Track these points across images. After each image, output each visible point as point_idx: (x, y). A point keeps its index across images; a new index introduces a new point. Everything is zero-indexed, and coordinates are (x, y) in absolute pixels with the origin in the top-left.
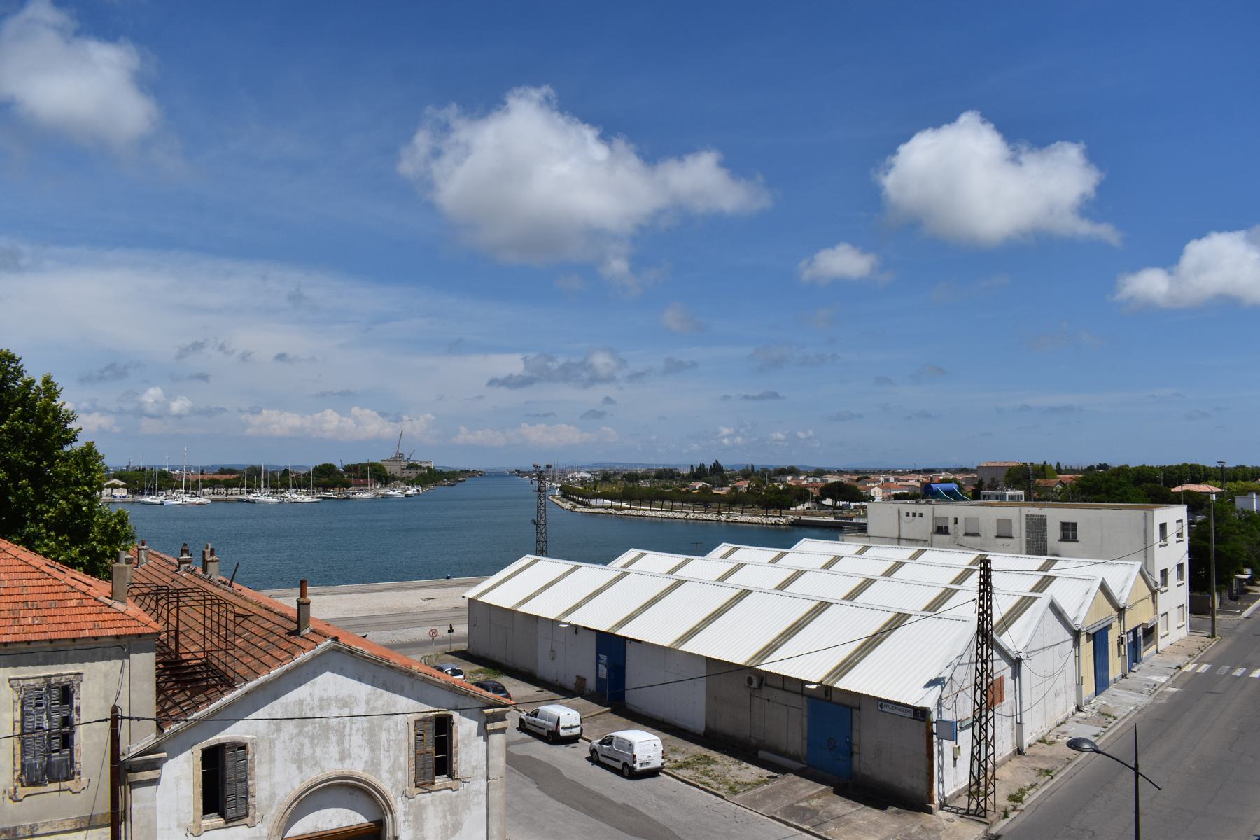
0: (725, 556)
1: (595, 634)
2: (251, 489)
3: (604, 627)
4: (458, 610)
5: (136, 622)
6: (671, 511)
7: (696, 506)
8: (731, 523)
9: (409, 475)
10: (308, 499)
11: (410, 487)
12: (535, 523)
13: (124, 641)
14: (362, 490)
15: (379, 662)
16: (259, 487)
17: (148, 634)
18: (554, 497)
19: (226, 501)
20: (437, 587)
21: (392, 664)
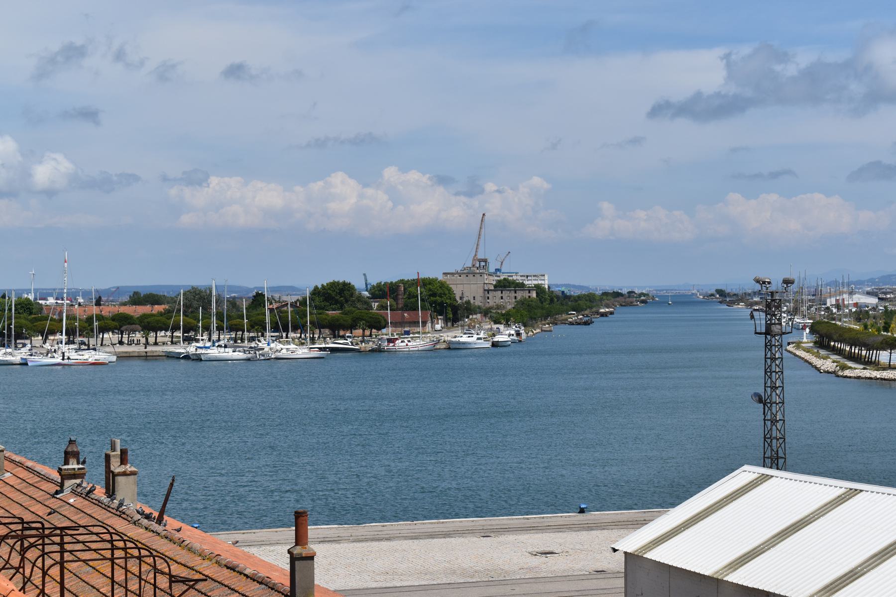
2: (192, 334)
9: (499, 302)
10: (302, 352)
11: (501, 327)
12: (760, 400)
14: (407, 333)
16: (207, 328)
19: (146, 357)
20: (560, 528)
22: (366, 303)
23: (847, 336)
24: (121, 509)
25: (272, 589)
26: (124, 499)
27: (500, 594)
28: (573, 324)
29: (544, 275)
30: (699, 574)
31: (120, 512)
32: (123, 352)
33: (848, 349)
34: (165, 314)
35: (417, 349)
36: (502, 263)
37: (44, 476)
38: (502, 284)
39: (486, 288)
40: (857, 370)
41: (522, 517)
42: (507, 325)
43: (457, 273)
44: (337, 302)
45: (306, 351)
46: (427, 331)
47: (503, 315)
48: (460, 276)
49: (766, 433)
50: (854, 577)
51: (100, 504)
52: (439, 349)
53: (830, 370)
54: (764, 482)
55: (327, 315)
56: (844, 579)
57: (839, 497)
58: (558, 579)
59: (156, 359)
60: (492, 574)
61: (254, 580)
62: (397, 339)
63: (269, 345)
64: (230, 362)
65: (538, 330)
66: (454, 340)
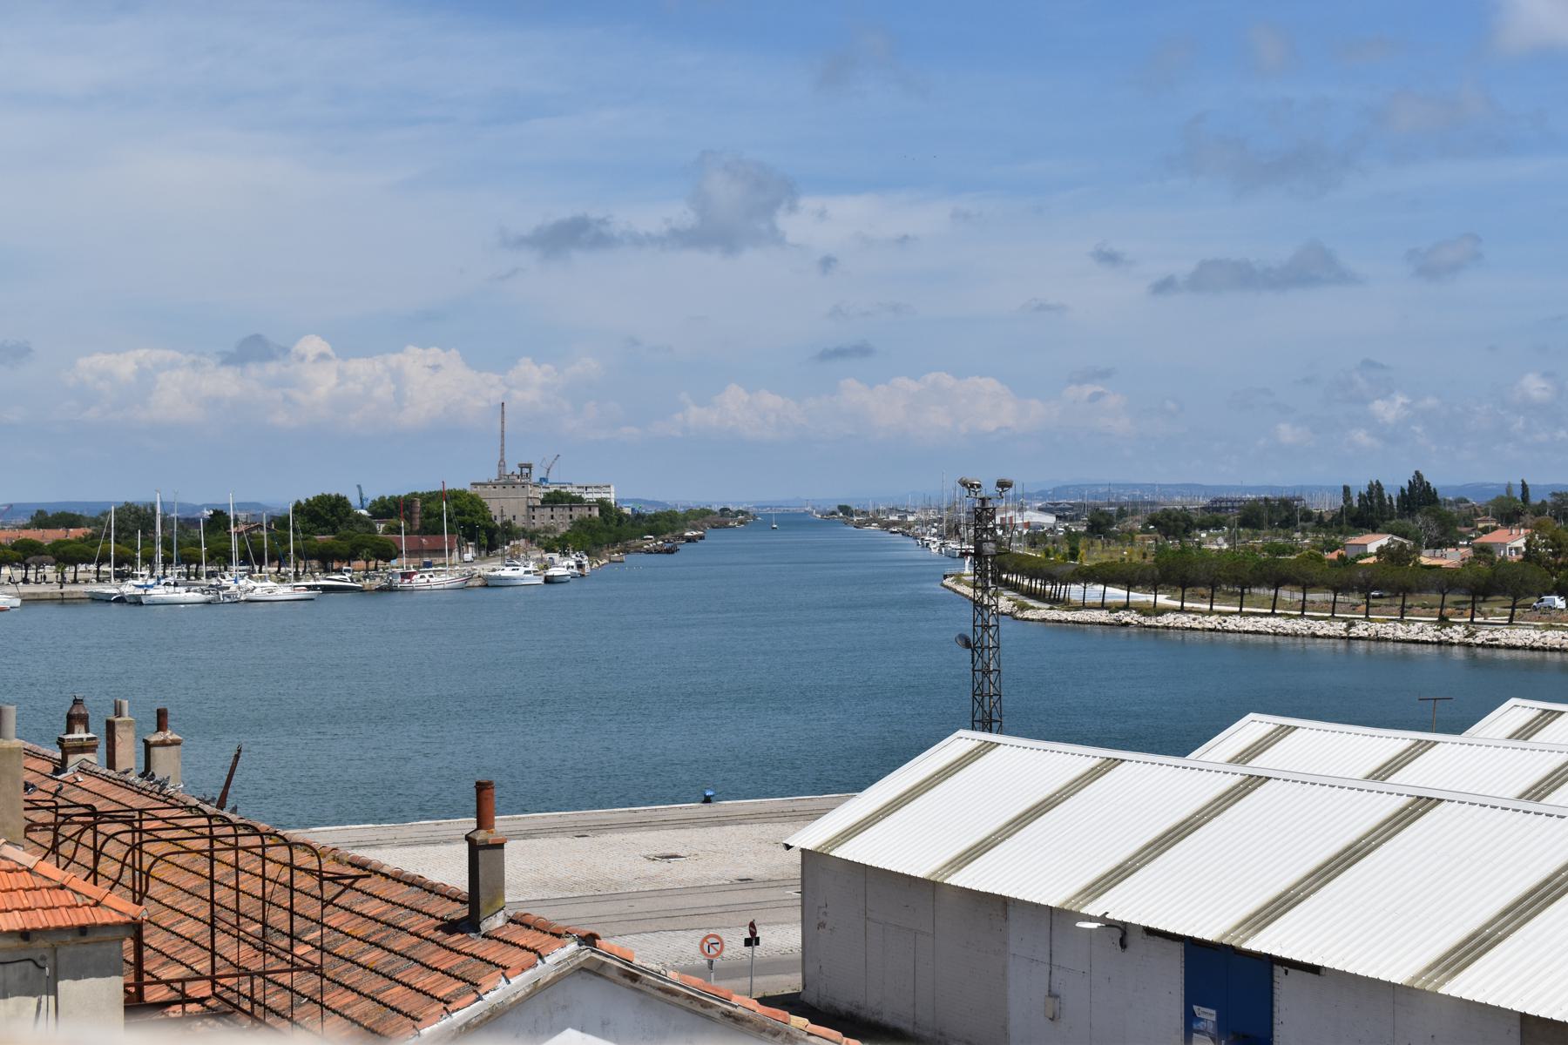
0: (1525, 733)
1: (1178, 948)
2: (126, 568)
3: (1209, 930)
4: (749, 885)
5: (69, 893)
6: (1302, 616)
7: (1372, 601)
8: (1479, 650)
9: (548, 522)
10: (283, 592)
11: (556, 556)
12: (967, 644)
13: (42, 944)
14: (428, 565)
15: (705, 1005)
16: (149, 560)
17: (106, 925)
18: (959, 579)
19: (62, 601)
20: (682, 824)
21: (740, 1011)
22: (367, 524)
23: (1026, 565)
24: (165, 792)
25: (431, 892)
26: (168, 778)
27: (615, 913)
28: (651, 553)
29: (609, 487)
30: (909, 877)
31: (164, 795)
32: (29, 594)
33: (1026, 582)
34: (86, 540)
35: (441, 586)
36: (549, 470)
37: (30, 751)
38: (552, 498)
39: (531, 504)
40: (1041, 611)
41: (627, 809)
42: (565, 554)
43: (490, 483)
44: (327, 523)
45: (289, 590)
46: (453, 562)
47: (556, 540)
48: (495, 487)
49: (975, 688)
50: (1123, 875)
51: (129, 786)
52: (473, 586)
53: (1006, 611)
54: (988, 751)
55: (316, 540)
56: (1110, 877)
57: (1093, 769)
58: (689, 891)
59: (76, 603)
60: (598, 885)
61: (399, 881)
62: (414, 573)
63: (236, 582)
64: (182, 606)
65: (605, 561)
66: (491, 574)
